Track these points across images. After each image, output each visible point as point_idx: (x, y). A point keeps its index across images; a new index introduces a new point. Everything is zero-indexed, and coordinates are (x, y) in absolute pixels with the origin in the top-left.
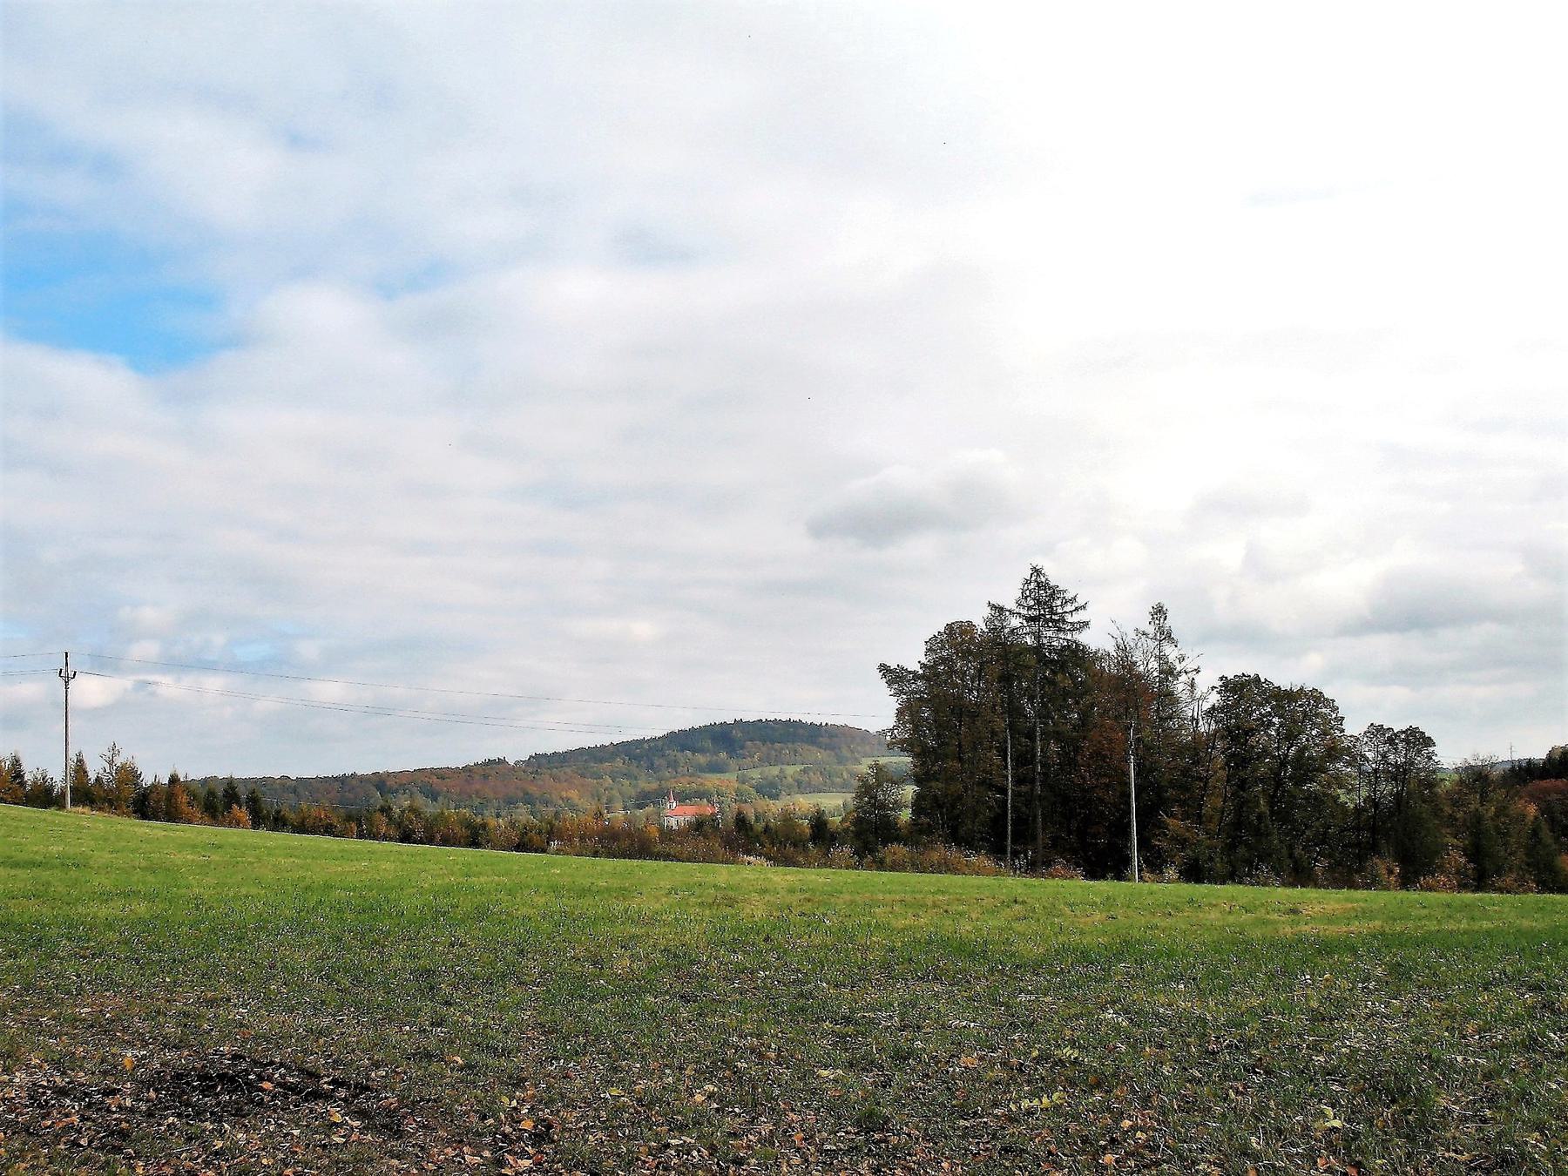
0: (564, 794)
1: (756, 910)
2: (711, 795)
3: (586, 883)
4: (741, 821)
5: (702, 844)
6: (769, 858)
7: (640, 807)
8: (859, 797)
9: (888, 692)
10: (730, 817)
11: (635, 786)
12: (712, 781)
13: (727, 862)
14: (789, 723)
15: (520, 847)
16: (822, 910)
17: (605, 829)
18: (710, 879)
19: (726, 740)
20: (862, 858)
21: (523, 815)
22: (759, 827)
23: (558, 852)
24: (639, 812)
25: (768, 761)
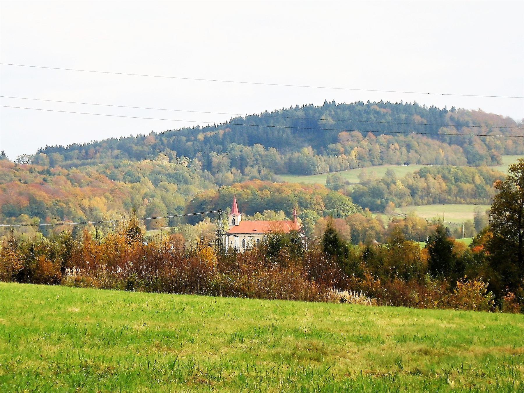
0: (86, 203)
1: (353, 364)
2: (291, 206)
3: (116, 325)
4: (332, 242)
5: (277, 273)
6: (370, 295)
7: (193, 221)
8: (497, 210)
9: (461, 108)
10: (317, 234)
11: (186, 193)
12: (292, 184)
13: (311, 299)
14: (397, 108)
15: (22, 277)
16: (445, 366)
17: (143, 252)
18: (289, 322)
19: (312, 129)
20: (499, 296)
21: (28, 232)
22: (357, 250)
23: (77, 283)
24: (189, 229)
25: (367, 159)
